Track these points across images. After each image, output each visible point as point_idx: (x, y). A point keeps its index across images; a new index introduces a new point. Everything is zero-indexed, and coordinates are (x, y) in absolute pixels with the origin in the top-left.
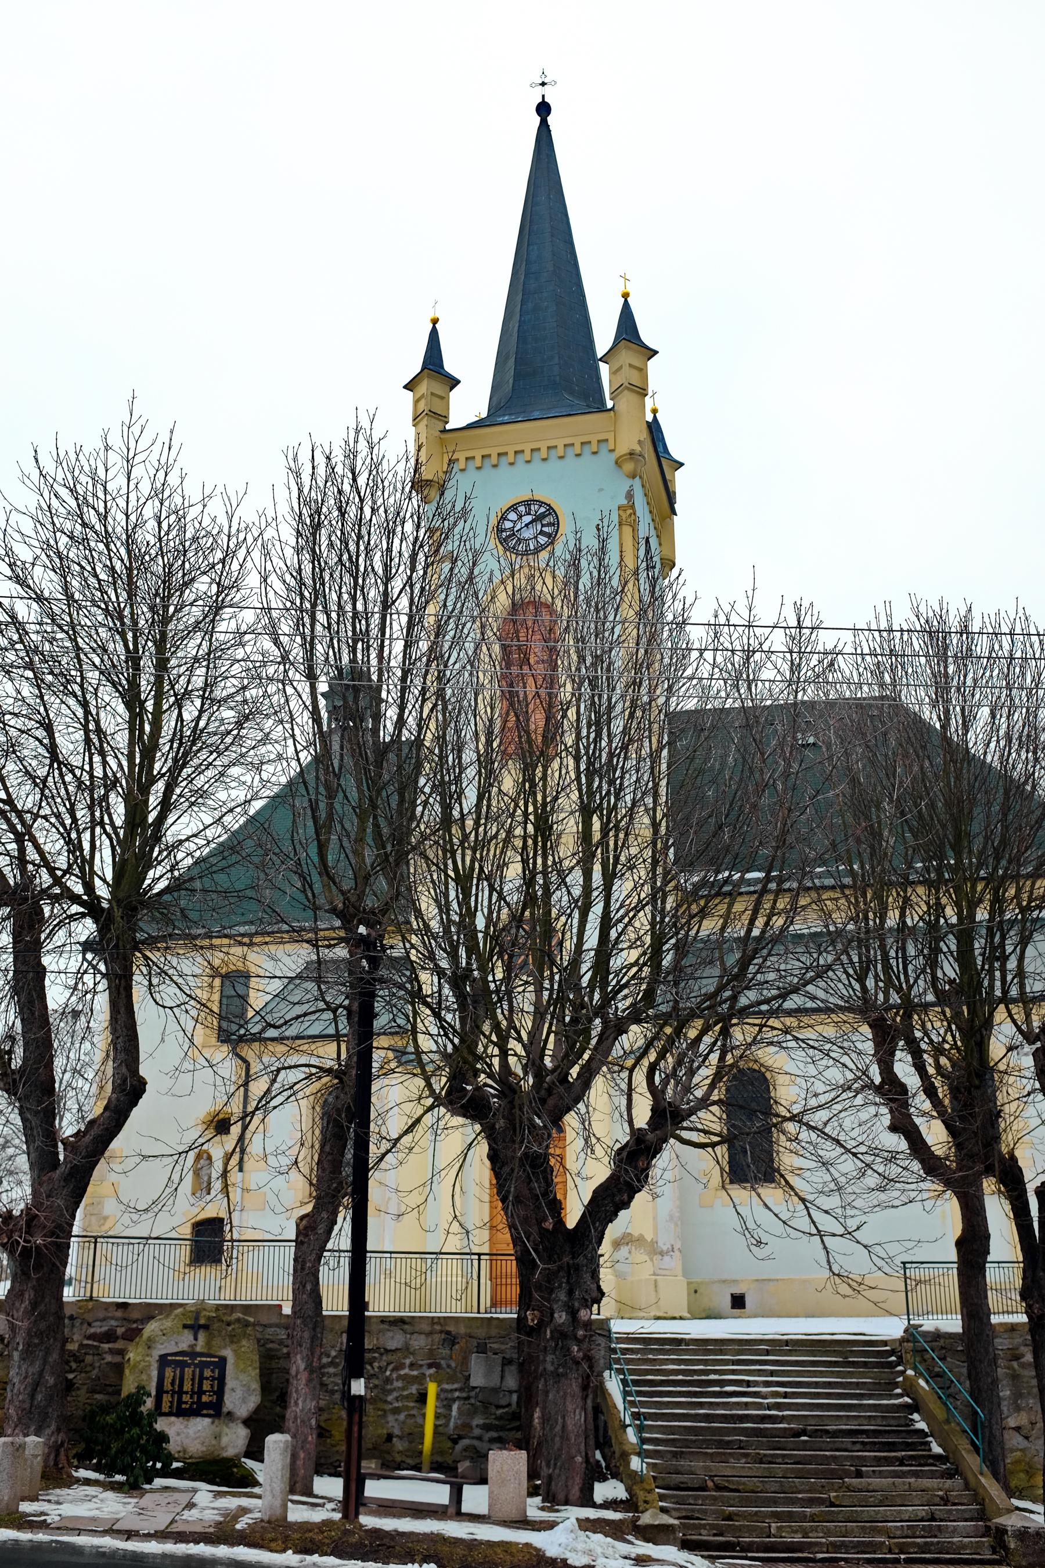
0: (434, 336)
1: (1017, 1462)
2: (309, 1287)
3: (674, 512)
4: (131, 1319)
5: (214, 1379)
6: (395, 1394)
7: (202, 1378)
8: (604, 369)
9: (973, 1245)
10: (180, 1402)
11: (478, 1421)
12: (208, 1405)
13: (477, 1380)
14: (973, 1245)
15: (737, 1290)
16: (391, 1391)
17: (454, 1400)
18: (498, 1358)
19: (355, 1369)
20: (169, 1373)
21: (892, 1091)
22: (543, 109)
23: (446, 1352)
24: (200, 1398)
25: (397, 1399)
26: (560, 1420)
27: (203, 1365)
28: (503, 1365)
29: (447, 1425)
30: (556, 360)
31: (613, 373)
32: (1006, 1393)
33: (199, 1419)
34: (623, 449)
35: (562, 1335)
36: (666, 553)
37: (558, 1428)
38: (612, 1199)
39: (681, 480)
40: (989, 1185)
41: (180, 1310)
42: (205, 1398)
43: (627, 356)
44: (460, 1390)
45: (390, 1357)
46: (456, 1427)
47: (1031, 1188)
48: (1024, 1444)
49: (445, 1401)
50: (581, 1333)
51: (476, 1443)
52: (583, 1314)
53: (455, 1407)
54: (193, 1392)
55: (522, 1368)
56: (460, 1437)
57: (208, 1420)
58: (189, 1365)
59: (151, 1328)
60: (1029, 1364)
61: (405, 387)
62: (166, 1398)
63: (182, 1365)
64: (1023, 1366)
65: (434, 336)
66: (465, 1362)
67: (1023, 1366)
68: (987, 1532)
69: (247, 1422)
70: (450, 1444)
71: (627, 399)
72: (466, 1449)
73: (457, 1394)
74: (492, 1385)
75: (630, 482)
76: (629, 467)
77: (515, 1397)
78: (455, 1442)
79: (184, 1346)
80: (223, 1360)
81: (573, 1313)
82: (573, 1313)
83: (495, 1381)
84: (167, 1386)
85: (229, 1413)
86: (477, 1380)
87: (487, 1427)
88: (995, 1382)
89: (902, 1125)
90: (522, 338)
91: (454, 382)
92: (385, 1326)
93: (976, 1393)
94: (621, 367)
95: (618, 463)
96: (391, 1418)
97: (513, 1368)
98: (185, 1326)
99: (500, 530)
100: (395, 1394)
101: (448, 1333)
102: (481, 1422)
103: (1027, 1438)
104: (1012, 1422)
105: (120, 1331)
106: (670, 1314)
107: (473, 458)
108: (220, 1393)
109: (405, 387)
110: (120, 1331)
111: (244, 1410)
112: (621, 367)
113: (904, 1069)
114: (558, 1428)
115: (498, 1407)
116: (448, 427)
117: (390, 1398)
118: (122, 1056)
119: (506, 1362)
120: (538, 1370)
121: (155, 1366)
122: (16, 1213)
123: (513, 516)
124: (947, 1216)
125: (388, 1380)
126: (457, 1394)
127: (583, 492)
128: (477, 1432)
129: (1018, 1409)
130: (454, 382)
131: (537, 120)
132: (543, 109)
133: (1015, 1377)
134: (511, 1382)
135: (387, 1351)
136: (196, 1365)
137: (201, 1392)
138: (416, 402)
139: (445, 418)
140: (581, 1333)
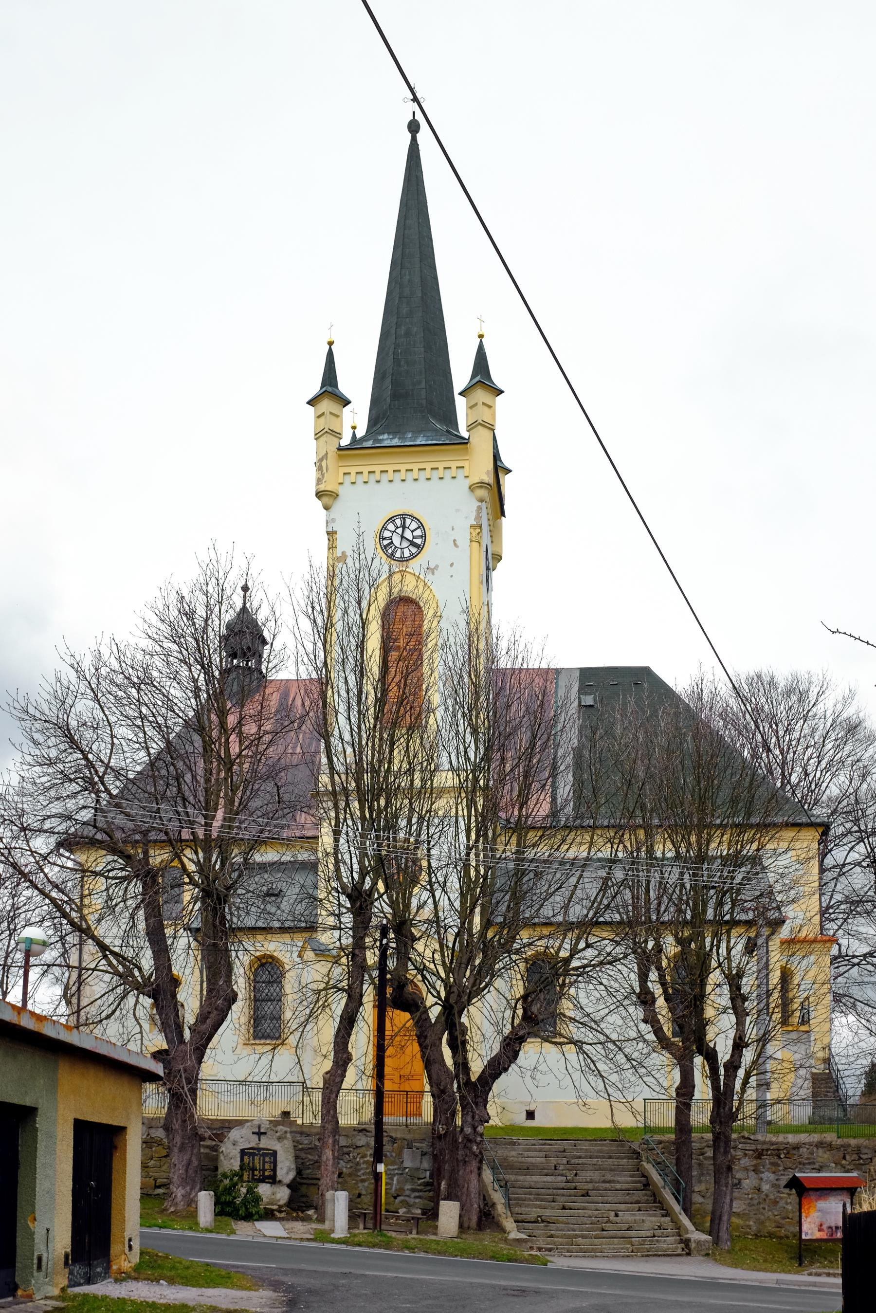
0: (330, 356)
1: (698, 1210)
2: (332, 1112)
3: (503, 514)
4: (222, 1128)
5: (271, 1163)
6: (362, 1172)
7: (264, 1162)
9: (686, 1090)
10: (253, 1175)
11: (408, 1186)
12: (269, 1177)
14: (686, 1090)
16: (359, 1170)
17: (394, 1175)
18: (419, 1152)
19: (378, 1156)
20: (246, 1159)
21: (645, 999)
24: (264, 1173)
25: (363, 1174)
26: (466, 1185)
27: (264, 1155)
28: (422, 1155)
29: (391, 1189)
30: (423, 385)
31: (471, 407)
32: (695, 1173)
33: (264, 1184)
35: (469, 1140)
36: (496, 550)
37: (465, 1189)
38: (497, 1068)
39: (507, 482)
40: (698, 1060)
41: (248, 1124)
42: (267, 1173)
43: (480, 395)
44: (398, 1169)
45: (358, 1151)
46: (396, 1190)
48: (701, 1200)
49: (390, 1176)
50: (479, 1139)
51: (407, 1198)
52: (480, 1129)
53: (395, 1179)
54: (260, 1170)
55: (435, 1158)
56: (398, 1195)
57: (269, 1185)
58: (257, 1155)
59: (234, 1134)
60: (709, 1157)
61: (308, 403)
63: (254, 1155)
64: (706, 1158)
65: (330, 356)
66: (400, 1154)
67: (706, 1158)
68: (681, 1241)
69: (289, 1186)
70: (392, 1199)
72: (401, 1202)
73: (396, 1172)
74: (415, 1166)
75: (480, 504)
77: (428, 1173)
78: (395, 1198)
79: (253, 1145)
80: (275, 1153)
81: (474, 1128)
82: (474, 1128)
83: (417, 1164)
85: (280, 1181)
86: (408, 1163)
87: (413, 1190)
88: (690, 1168)
89: (651, 1019)
90: (396, 362)
92: (356, 1133)
94: (476, 404)
95: (472, 488)
96: (360, 1185)
97: (427, 1157)
98: (253, 1133)
100: (362, 1172)
101: (391, 1137)
102: (410, 1187)
103: (703, 1197)
107: (362, 473)
108: (274, 1170)
109: (308, 403)
112: (476, 404)
113: (656, 989)
114: (465, 1189)
115: (419, 1179)
117: (359, 1174)
118: (345, 1023)
119: (424, 1154)
120: (443, 1160)
121: (239, 1155)
123: (391, 527)
124: (677, 1075)
125: (358, 1164)
126: (396, 1172)
127: (438, 495)
128: (407, 1193)
129: (700, 1182)
134: (426, 1164)
135: (357, 1147)
136: (261, 1155)
137: (264, 1170)
139: (338, 435)
140: (479, 1139)
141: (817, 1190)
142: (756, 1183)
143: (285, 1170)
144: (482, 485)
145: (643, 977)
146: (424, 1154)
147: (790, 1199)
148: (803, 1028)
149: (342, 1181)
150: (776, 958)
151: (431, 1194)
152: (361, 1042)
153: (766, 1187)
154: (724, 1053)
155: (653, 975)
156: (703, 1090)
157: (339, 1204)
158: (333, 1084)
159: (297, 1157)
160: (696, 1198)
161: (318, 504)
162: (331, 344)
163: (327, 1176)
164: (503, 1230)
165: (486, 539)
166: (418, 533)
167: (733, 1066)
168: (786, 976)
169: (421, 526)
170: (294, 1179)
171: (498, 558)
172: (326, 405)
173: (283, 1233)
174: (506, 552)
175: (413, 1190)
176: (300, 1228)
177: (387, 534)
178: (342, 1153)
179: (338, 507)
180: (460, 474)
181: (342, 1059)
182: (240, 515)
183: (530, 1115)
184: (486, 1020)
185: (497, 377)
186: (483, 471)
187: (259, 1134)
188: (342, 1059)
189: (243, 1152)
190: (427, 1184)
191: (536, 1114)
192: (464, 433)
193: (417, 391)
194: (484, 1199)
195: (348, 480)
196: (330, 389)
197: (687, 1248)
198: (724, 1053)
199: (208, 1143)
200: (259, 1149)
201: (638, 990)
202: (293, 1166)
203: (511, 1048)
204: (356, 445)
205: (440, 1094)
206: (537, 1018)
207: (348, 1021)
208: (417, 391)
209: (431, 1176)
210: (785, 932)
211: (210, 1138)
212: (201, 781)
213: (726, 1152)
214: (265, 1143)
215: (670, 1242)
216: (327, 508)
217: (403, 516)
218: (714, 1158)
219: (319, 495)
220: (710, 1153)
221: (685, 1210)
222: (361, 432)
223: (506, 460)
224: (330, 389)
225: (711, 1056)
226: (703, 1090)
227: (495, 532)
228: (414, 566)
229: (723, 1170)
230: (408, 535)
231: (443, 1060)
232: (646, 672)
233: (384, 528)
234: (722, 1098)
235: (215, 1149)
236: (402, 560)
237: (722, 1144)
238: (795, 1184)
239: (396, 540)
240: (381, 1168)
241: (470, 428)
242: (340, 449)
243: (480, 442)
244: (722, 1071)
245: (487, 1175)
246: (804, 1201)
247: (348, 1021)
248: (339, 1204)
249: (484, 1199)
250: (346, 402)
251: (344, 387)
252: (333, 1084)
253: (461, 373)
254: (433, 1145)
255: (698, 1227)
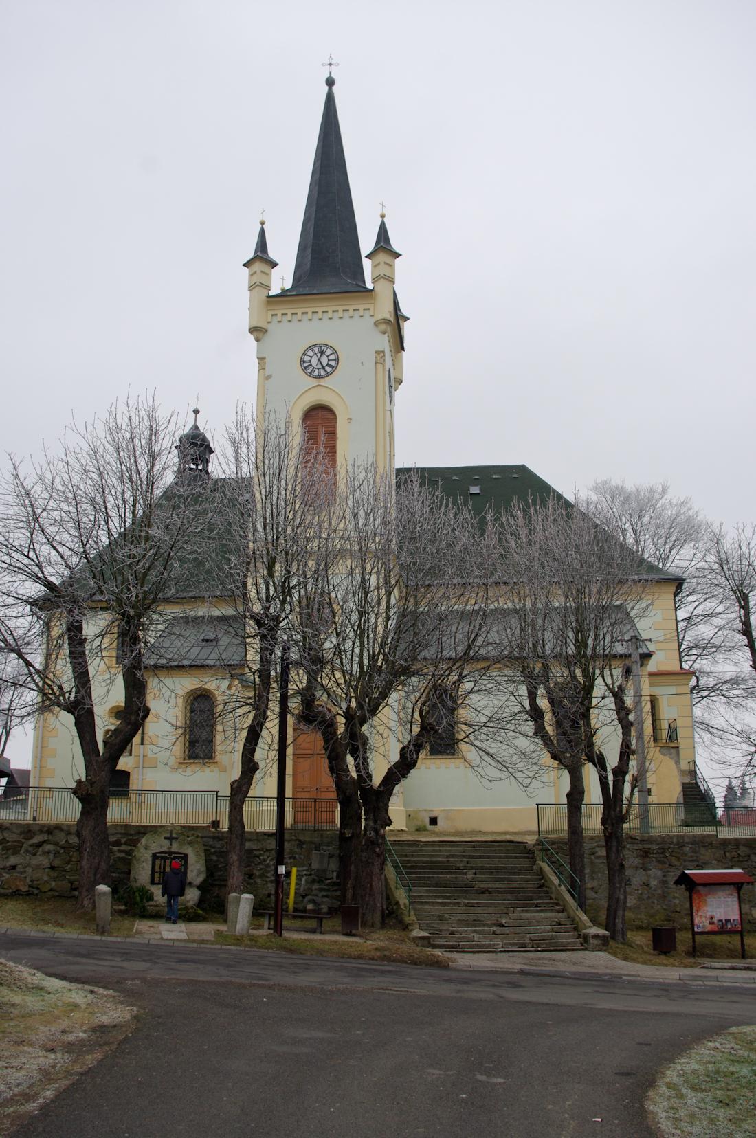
0: (262, 233)
8: (367, 265)
9: (576, 797)
13: (315, 865)
14: (576, 797)
15: (433, 815)
19: (280, 861)
20: (158, 863)
21: (536, 714)
22: (330, 82)
23: (298, 850)
31: (375, 266)
32: (587, 871)
34: (379, 316)
35: (372, 843)
36: (398, 376)
39: (407, 328)
43: (382, 257)
47: (609, 769)
49: (299, 877)
62: (157, 876)
63: (165, 858)
64: (598, 857)
65: (262, 233)
67: (598, 857)
69: (198, 888)
71: (382, 284)
76: (383, 327)
79: (165, 849)
80: (186, 856)
84: (157, 869)
86: (315, 865)
87: (321, 890)
88: (583, 866)
89: (540, 731)
90: (316, 235)
91: (274, 265)
93: (574, 869)
95: (376, 324)
99: (302, 361)
104: (589, 885)
105: (123, 840)
106: (166, 796)
110: (123, 840)
111: (198, 880)
113: (543, 703)
116: (271, 294)
122: (84, 779)
123: (310, 353)
124: (565, 782)
127: (345, 328)
129: (593, 879)
130: (274, 265)
131: (326, 88)
132: (330, 82)
133: (592, 863)
134: (334, 865)
138: (251, 275)
139: (268, 288)
141: (705, 885)
142: (643, 880)
143: (195, 873)
144: (386, 321)
145: (532, 696)
146: (330, 856)
147: (680, 893)
148: (672, 745)
149: (249, 884)
150: (645, 683)
151: (338, 893)
152: (265, 755)
153: (654, 883)
154: (612, 761)
155: (541, 691)
156: (593, 794)
157: (244, 904)
158: (240, 790)
159: (208, 861)
160: (590, 894)
161: (251, 338)
162: (262, 223)
163: (236, 877)
164: (406, 927)
165: (389, 364)
166: (332, 357)
167: (620, 772)
168: (654, 701)
169: (335, 352)
170: (205, 880)
171: (399, 381)
172: (258, 266)
173: (183, 936)
174: (405, 378)
175: (321, 890)
176: (205, 930)
177: (307, 358)
178: (250, 858)
179: (267, 339)
180: (367, 314)
181: (249, 767)
182: (204, 371)
183: (433, 821)
184: (387, 736)
185: (396, 245)
186: (386, 312)
187: (170, 839)
188: (249, 767)
189: (155, 856)
190: (334, 884)
191: (439, 821)
192: (369, 285)
193: (333, 254)
194: (388, 898)
195: (275, 319)
196: (261, 256)
197: (584, 942)
198: (612, 761)
199: (123, 847)
200: (170, 853)
201: (528, 707)
202: (204, 869)
203: (405, 766)
204: (284, 294)
205: (346, 801)
206: (437, 735)
207: (254, 735)
208: (333, 254)
209: (338, 877)
210: (652, 666)
211: (125, 844)
212: (162, 562)
213: (618, 852)
214: (175, 847)
215: (565, 937)
216: (257, 340)
217: (320, 346)
218: (608, 857)
219: (252, 330)
220: (603, 852)
221: (581, 905)
222: (288, 285)
223: (405, 310)
224: (261, 256)
225: (600, 762)
226: (593, 794)
227: (397, 362)
228: (327, 382)
229: (616, 870)
230: (324, 361)
231: (127, 688)
232: (522, 469)
233: (305, 354)
234: (612, 801)
235: (129, 853)
236: (319, 377)
237: (614, 843)
238: (684, 880)
239: (314, 361)
240: (282, 870)
241: (374, 280)
242: (269, 297)
243: (382, 289)
244: (611, 777)
245: (390, 871)
246: (695, 896)
247: (254, 735)
248: (244, 904)
249: (388, 898)
250: (274, 265)
251: (272, 254)
252: (240, 790)
253: (367, 243)
254: (340, 847)
255: (595, 922)
